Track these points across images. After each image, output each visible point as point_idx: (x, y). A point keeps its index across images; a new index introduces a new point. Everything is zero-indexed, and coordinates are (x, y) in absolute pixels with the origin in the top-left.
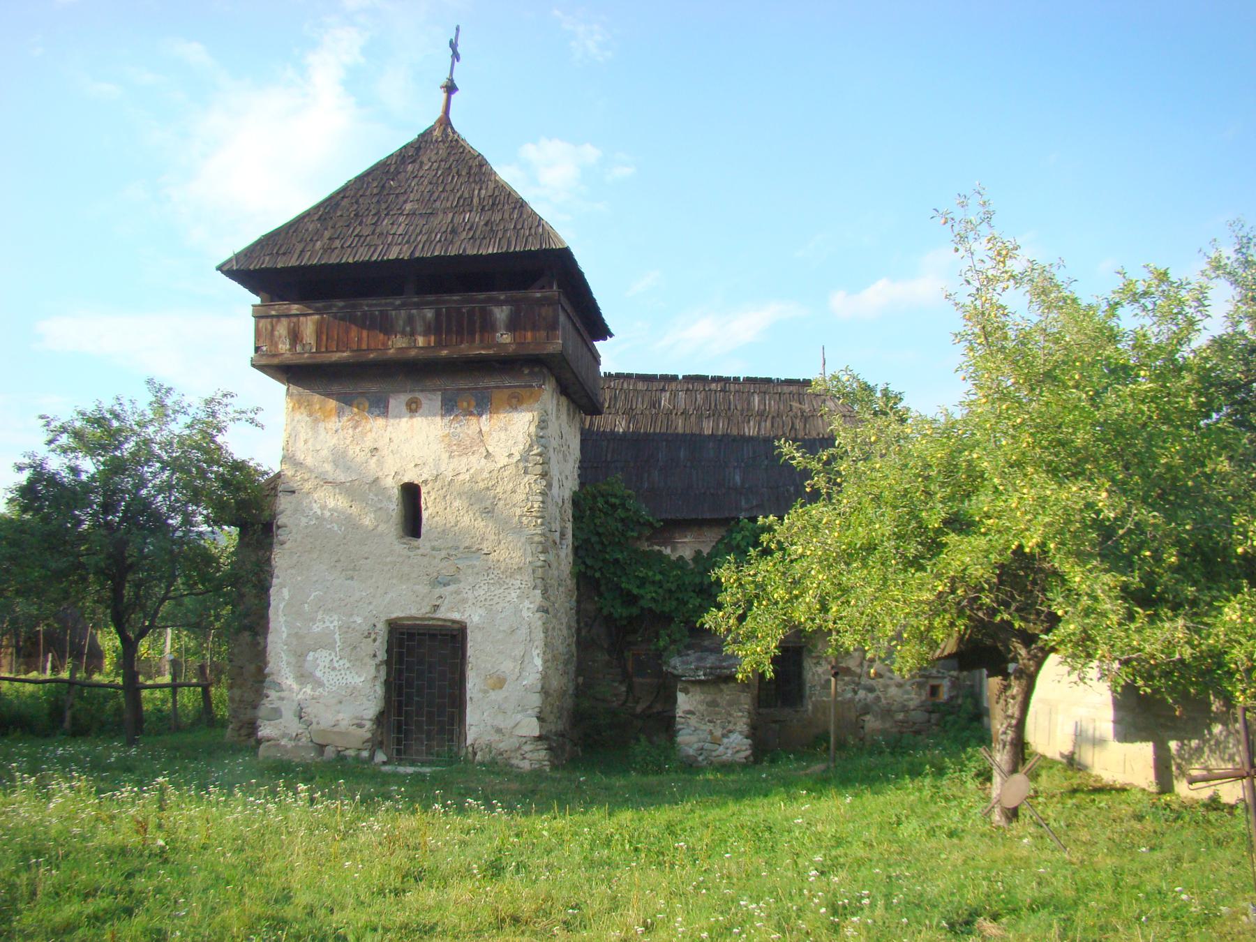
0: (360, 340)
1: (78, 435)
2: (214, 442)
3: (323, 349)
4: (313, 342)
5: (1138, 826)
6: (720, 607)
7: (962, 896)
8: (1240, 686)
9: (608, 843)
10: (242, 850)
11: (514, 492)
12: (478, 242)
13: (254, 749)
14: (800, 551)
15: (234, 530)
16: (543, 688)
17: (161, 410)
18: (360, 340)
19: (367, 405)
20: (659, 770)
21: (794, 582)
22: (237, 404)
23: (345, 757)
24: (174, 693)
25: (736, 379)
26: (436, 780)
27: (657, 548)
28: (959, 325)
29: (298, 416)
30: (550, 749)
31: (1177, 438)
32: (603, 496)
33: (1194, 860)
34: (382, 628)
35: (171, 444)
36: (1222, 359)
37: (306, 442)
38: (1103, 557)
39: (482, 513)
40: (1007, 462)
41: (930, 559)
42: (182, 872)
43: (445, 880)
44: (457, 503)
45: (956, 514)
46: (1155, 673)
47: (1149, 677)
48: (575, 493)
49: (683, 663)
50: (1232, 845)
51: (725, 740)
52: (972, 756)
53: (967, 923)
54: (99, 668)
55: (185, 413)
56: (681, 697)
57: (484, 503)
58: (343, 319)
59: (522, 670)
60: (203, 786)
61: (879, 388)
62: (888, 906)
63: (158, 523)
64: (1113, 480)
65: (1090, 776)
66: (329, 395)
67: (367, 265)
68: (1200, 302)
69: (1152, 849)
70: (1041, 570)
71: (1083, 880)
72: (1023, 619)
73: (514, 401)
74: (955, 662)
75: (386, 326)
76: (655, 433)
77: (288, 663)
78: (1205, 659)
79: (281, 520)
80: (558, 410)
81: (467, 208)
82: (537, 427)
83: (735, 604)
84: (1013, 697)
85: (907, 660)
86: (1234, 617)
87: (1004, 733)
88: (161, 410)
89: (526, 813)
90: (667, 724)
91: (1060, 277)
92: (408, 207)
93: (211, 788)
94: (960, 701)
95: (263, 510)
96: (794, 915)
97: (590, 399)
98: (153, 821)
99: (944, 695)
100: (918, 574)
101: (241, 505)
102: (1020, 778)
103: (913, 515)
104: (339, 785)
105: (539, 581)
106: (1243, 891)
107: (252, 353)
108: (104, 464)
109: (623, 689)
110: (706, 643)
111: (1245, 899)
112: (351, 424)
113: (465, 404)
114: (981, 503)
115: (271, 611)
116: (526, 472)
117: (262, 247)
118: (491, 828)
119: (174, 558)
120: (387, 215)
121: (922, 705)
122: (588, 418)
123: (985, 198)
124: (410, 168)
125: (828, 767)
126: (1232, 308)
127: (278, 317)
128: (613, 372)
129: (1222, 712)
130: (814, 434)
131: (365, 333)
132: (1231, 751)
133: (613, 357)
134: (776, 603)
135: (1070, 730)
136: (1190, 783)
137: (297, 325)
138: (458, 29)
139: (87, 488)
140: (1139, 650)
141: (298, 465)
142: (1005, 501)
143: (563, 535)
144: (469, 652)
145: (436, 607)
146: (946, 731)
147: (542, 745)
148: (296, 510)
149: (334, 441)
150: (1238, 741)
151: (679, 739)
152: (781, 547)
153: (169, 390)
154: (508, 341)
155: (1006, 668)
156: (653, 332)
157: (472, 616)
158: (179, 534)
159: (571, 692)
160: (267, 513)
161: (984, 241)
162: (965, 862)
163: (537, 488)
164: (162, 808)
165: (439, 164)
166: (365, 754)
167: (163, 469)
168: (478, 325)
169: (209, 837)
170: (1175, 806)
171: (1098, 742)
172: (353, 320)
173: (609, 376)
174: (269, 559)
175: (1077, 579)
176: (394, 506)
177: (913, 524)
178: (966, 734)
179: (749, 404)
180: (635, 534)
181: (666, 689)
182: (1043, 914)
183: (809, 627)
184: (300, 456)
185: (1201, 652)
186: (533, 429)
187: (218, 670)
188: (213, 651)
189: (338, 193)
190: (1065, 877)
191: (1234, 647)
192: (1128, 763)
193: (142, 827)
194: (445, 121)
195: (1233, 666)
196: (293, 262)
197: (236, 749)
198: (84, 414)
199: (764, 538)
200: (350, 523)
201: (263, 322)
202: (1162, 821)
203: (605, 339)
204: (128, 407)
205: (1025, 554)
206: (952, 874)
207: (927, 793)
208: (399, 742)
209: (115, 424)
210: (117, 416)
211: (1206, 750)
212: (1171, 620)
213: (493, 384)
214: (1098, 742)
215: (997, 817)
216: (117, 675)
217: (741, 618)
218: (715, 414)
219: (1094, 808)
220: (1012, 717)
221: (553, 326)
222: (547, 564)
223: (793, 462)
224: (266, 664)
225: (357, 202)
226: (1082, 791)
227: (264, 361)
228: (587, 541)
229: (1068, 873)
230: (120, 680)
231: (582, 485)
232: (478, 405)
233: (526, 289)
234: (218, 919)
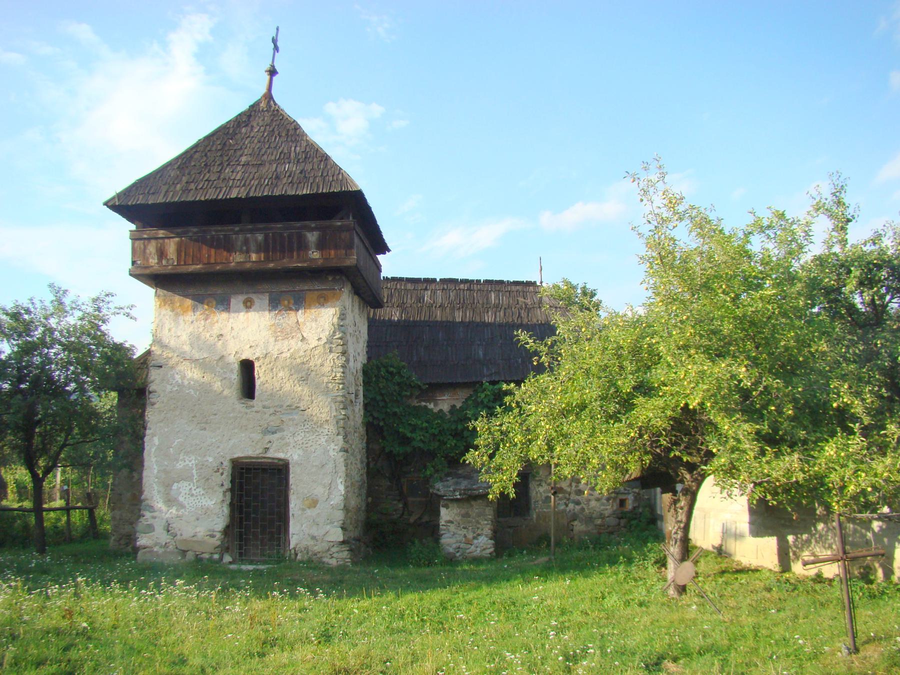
0: (209, 256)
3: (182, 263)
4: (175, 258)
5: (768, 595)
6: (476, 448)
7: (652, 646)
8: (835, 499)
9: (402, 616)
11: (322, 365)
12: (295, 186)
14: (534, 409)
15: (114, 394)
16: (345, 506)
17: (60, 308)
18: (209, 256)
19: (214, 303)
20: (430, 563)
21: (528, 430)
22: (116, 302)
23: (201, 559)
25: (478, 281)
27: (423, 404)
28: (643, 251)
29: (164, 312)
30: (351, 550)
31: (792, 327)
32: (385, 367)
33: (807, 617)
34: (227, 465)
36: (821, 272)
37: (170, 330)
38: (744, 412)
39: (299, 381)
40: (677, 346)
41: (624, 414)
44: (281, 374)
45: (642, 382)
46: (780, 490)
47: (775, 494)
49: (444, 486)
50: (831, 606)
51: (475, 541)
52: (652, 549)
53: (657, 664)
54: (5, 496)
55: (80, 310)
56: (443, 511)
57: (303, 373)
58: (197, 241)
59: (330, 494)
60: (106, 583)
61: (580, 286)
62: (603, 653)
63: (57, 391)
64: (748, 358)
65: (733, 561)
66: (186, 296)
67: (215, 202)
68: (807, 234)
69: (778, 611)
70: (701, 420)
71: (733, 633)
72: (690, 454)
73: (322, 300)
74: (638, 483)
75: (228, 246)
77: (159, 492)
78: (812, 480)
79: (152, 387)
80: (353, 306)
81: (286, 161)
82: (339, 318)
83: (487, 446)
84: (682, 508)
85: (606, 482)
86: (832, 453)
87: (676, 533)
88: (60, 308)
89: (340, 597)
90: (433, 530)
91: (712, 216)
92: (244, 159)
94: (640, 510)
96: (539, 662)
99: (629, 505)
100: (616, 425)
101: (121, 376)
102: (688, 564)
103: (612, 383)
104: (205, 580)
105: (341, 429)
106: (839, 637)
107: (130, 266)
108: (18, 345)
109: (401, 505)
110: (460, 472)
111: (840, 642)
112: (203, 317)
113: (286, 302)
114: (658, 374)
116: (331, 351)
117: (137, 188)
120: (228, 165)
121: (614, 513)
122: (372, 310)
123: (661, 163)
124: (244, 130)
125: (550, 559)
126: (827, 236)
127: (149, 239)
129: (824, 515)
130: (535, 321)
131: (213, 251)
132: (830, 542)
133: (390, 266)
134: (516, 445)
135: (718, 529)
136: (804, 565)
137: (163, 245)
138: (278, 29)
140: (769, 476)
141: (164, 346)
142: (676, 373)
143: (356, 396)
144: (291, 481)
145: (267, 449)
146: (631, 532)
147: (345, 548)
148: (163, 380)
149: (191, 329)
150: (835, 535)
152: (518, 405)
153: (65, 292)
154: (317, 257)
155: (675, 487)
156: (420, 246)
158: (73, 397)
159: (363, 508)
161: (661, 193)
162: (652, 623)
163: (339, 362)
165: (263, 127)
166: (216, 556)
168: (295, 245)
170: (792, 581)
171: (738, 536)
172: (204, 241)
174: (142, 416)
175: (726, 427)
176: (235, 376)
177: (612, 390)
178: (647, 533)
179: (487, 299)
180: (408, 394)
181: (432, 505)
182: (708, 656)
183: (540, 462)
184: (166, 340)
185: (810, 476)
186: (335, 320)
190: (721, 631)
191: (831, 473)
192: (760, 552)
194: (269, 96)
195: (831, 485)
196: (160, 199)
197: (117, 555)
200: (204, 389)
201: (137, 243)
202: (784, 591)
203: (385, 253)
204: (38, 305)
205: (689, 409)
206: (643, 631)
207: (621, 576)
209: (26, 317)
210: (28, 311)
211: (813, 541)
212: (789, 454)
213: (306, 288)
214: (738, 536)
215: (671, 592)
217: (491, 456)
218: (463, 306)
219: (737, 584)
220: (681, 522)
221: (350, 246)
222: (347, 417)
223: (527, 346)
224: (141, 492)
225: (206, 155)
226: (729, 572)
227: (138, 272)
228: (374, 399)
229: (723, 629)
231: (369, 359)
232: (296, 303)
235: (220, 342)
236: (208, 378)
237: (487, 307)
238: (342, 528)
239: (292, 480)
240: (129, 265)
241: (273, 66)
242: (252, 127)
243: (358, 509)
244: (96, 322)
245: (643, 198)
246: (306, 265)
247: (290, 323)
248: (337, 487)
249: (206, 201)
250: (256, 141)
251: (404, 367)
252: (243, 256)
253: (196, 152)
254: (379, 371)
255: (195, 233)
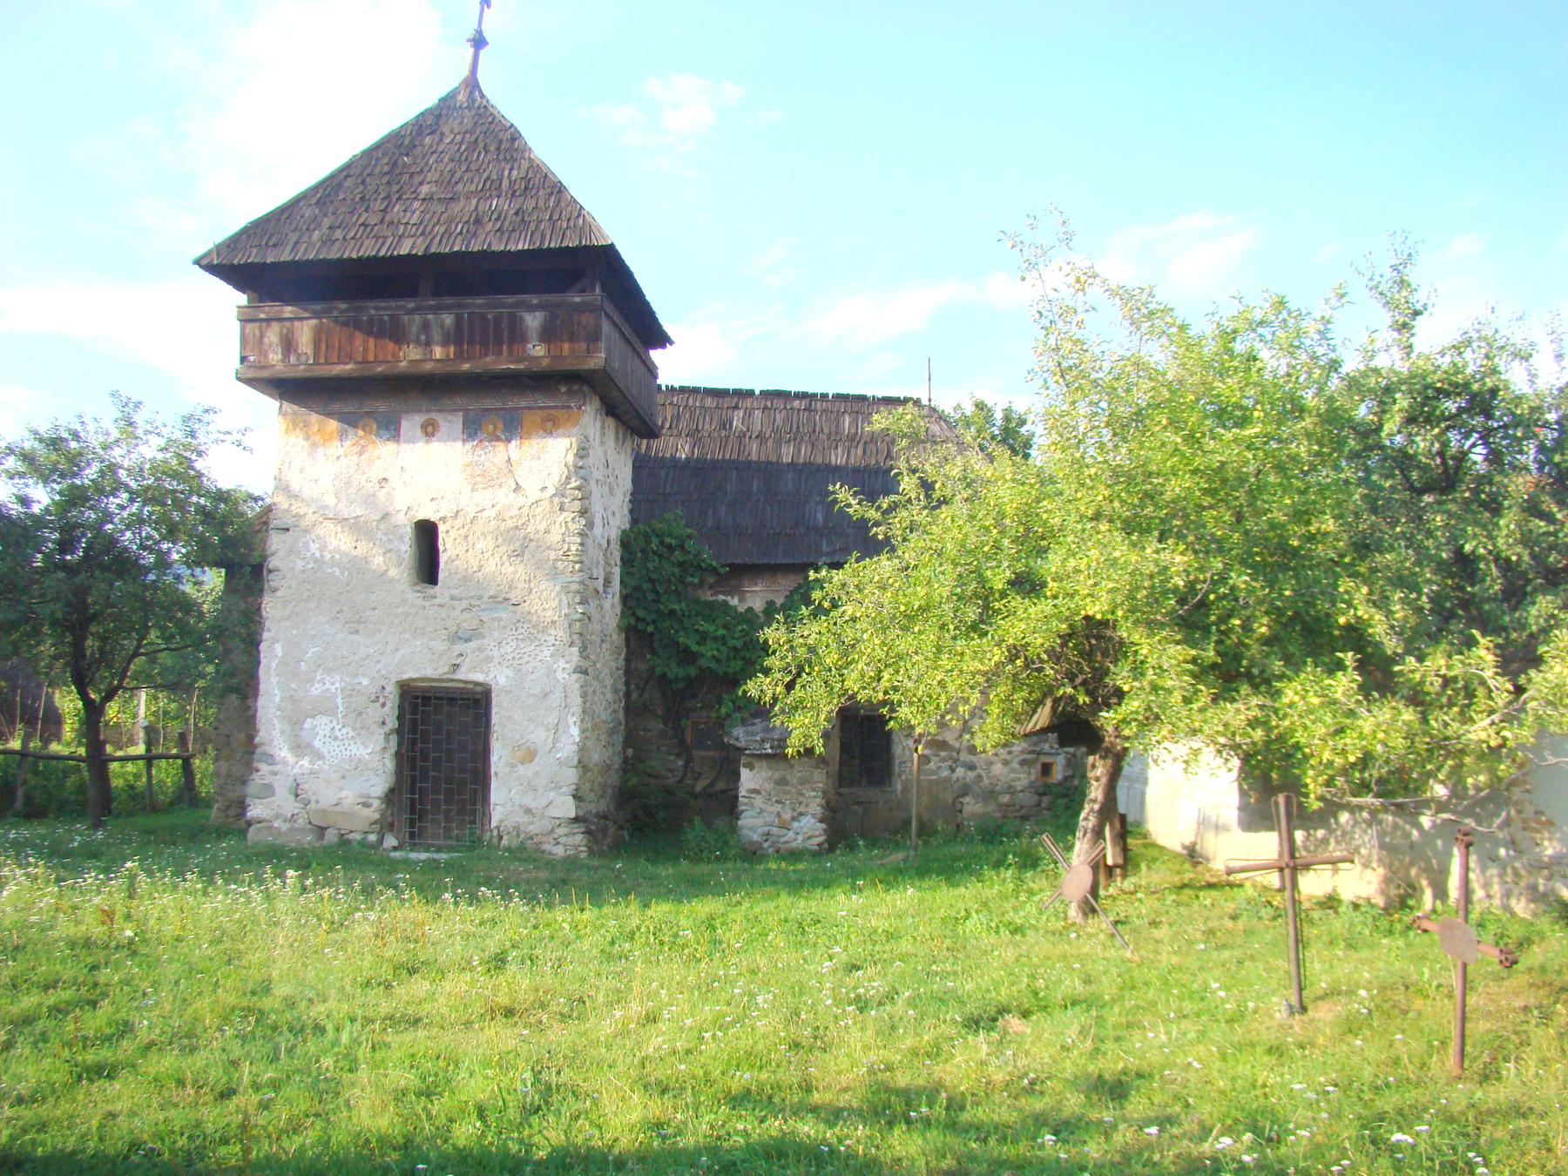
0: (366, 350)
1: (28, 458)
2: (193, 468)
4: (310, 352)
6: (767, 672)
10: (220, 942)
11: (547, 532)
13: (243, 833)
18: (366, 350)
19: (375, 426)
22: (219, 422)
23: (349, 842)
24: (149, 767)
25: (824, 396)
26: (450, 867)
27: (721, 597)
30: (588, 832)
34: (392, 693)
35: (141, 470)
37: (302, 470)
42: (152, 964)
43: (442, 973)
44: (480, 546)
48: (624, 532)
49: (747, 733)
51: (795, 824)
54: (58, 737)
56: (745, 773)
57: (521, 545)
58: (346, 324)
60: (180, 873)
63: (124, 565)
66: (329, 415)
73: (549, 424)
75: (397, 334)
76: (723, 460)
77: (282, 732)
79: (273, 563)
81: (494, 193)
82: (576, 455)
90: (729, 804)
92: (425, 189)
93: (189, 876)
95: (252, 550)
97: (639, 417)
98: (120, 910)
99: (1058, 774)
101: (228, 542)
103: (978, 572)
105: (575, 637)
107: (237, 364)
109: (681, 763)
112: (356, 449)
113: (491, 427)
114: (1051, 564)
115: (262, 671)
116: (562, 509)
118: (510, 920)
119: (146, 606)
121: (1031, 785)
124: (428, 140)
128: (676, 386)
131: (372, 342)
139: (39, 522)
143: (607, 582)
144: (495, 719)
145: (456, 666)
151: (740, 823)
153: (138, 405)
157: (498, 677)
158: (151, 577)
159: (617, 766)
160: (256, 554)
164: (131, 897)
165: (463, 139)
166: (373, 838)
167: (132, 500)
168: (506, 333)
169: (183, 928)
171: (1218, 828)
172: (358, 326)
173: (672, 390)
174: (259, 609)
176: (406, 546)
180: (696, 580)
186: (570, 458)
187: (204, 739)
188: (198, 713)
189: (341, 170)
193: (108, 916)
194: (472, 83)
196: (286, 256)
197: (221, 833)
198: (36, 433)
199: (816, 595)
200: (357, 566)
201: (249, 326)
203: (664, 347)
204: (91, 427)
208: (412, 824)
209: (73, 445)
210: (76, 436)
211: (1332, 841)
213: (523, 404)
214: (1218, 828)
216: (80, 744)
217: (790, 687)
218: (797, 438)
221: (594, 337)
225: (363, 182)
227: (251, 374)
228: (637, 588)
230: (82, 751)
231: (634, 521)
233: (563, 291)
234: (190, 1011)
235: (384, 491)
236: (363, 548)
237: (835, 439)
238: (574, 797)
239: (495, 718)
240: (236, 363)
241: (479, 32)
242: (442, 134)
243: (607, 769)
244: (187, 454)
245: (1027, 275)
246: (521, 367)
247: (496, 460)
248: (566, 731)
249: (359, 259)
250: (446, 159)
251: (690, 537)
252: (420, 350)
253: (347, 176)
254: (648, 541)
255: (346, 311)
